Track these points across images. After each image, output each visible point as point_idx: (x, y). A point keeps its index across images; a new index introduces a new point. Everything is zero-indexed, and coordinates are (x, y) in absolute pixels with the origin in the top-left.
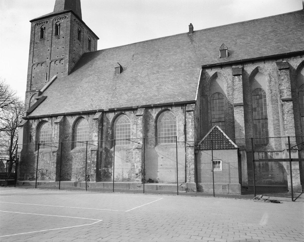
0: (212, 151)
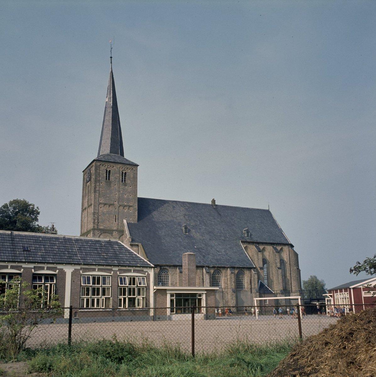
0: (66, 308)
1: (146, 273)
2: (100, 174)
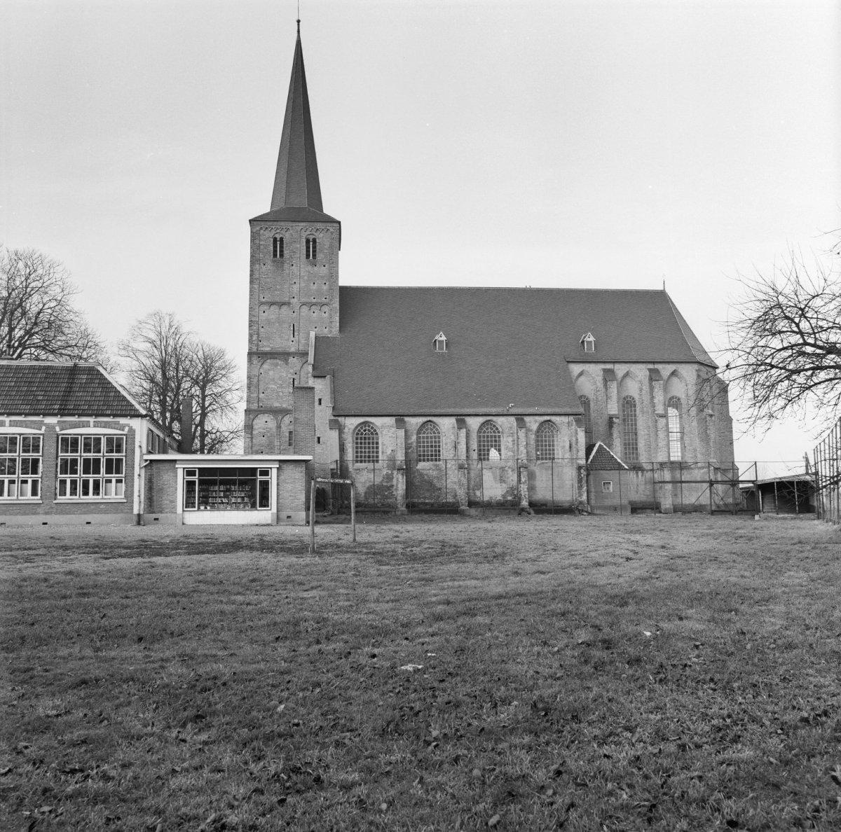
1: (127, 429)
2: (262, 247)
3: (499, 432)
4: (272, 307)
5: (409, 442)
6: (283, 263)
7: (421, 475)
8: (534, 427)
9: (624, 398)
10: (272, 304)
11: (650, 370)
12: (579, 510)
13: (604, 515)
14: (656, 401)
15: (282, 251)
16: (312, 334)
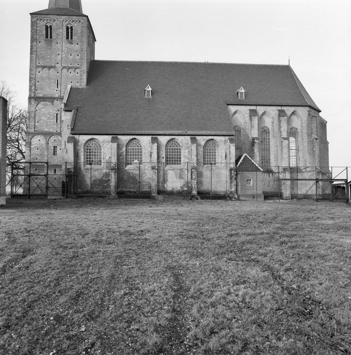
2: (38, 31)
3: (180, 146)
4: (44, 69)
5: (121, 152)
6: (51, 41)
7: (129, 173)
8: (203, 143)
9: (263, 128)
10: (44, 67)
11: (279, 111)
12: (230, 198)
13: (246, 200)
14: (282, 129)
15: (51, 35)
16: (69, 87)
